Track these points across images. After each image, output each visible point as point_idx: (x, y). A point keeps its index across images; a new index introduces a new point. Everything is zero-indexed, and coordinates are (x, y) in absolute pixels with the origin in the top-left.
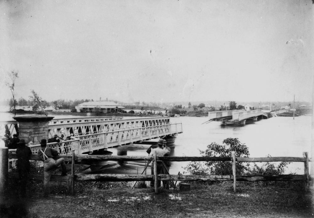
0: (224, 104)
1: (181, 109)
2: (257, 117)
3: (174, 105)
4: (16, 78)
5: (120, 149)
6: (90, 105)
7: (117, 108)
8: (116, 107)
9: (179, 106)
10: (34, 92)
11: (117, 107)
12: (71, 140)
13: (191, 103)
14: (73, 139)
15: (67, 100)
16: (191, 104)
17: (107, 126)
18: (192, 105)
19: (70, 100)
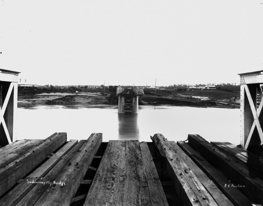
11: (33, 86)
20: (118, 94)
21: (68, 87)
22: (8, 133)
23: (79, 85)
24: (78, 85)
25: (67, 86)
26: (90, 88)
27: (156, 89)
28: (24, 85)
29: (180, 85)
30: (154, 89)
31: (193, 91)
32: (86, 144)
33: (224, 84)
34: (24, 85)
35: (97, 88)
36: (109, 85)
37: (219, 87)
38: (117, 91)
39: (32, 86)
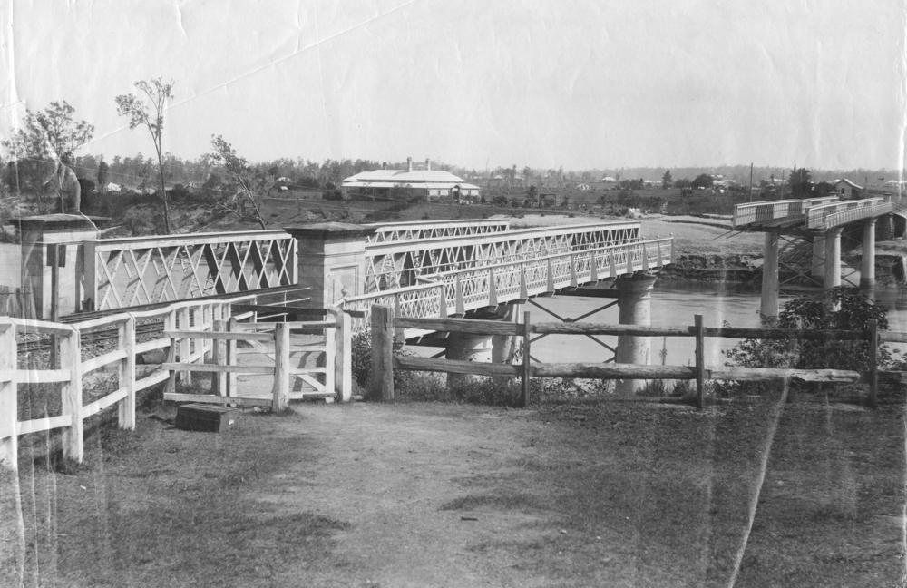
0: (772, 177)
1: (640, 191)
2: (876, 218)
3: (618, 177)
4: (661, 364)
5: (126, 190)
6: (678, 221)
7: (456, 189)
8: (454, 185)
9: (634, 181)
10: (445, 508)
11: (456, 187)
12: (417, 286)
13: (671, 173)
14: (422, 282)
15: (300, 162)
16: (672, 178)
17: (489, 247)
18: (674, 179)
19: (309, 163)
28: (424, 182)
29: (511, 168)
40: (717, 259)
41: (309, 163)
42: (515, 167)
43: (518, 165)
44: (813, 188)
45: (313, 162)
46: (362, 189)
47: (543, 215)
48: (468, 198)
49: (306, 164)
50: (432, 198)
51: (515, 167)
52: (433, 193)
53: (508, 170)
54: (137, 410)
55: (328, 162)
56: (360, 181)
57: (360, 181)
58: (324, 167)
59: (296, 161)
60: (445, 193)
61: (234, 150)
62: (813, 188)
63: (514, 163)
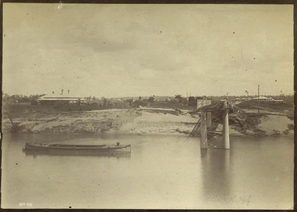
11: (79, 100)
20: (200, 108)
21: (120, 100)
22: (169, 209)
23: (140, 97)
24: (139, 96)
25: (119, 99)
26: (158, 101)
27: (268, 100)
28: (68, 98)
29: (89, 97)
30: (264, 100)
31: (17, 100)
32: (25, 125)
33: (94, 98)
34: (68, 98)
35: (170, 102)
36: (189, 96)
37: (111, 99)
38: (198, 105)
39: (78, 99)
40: (115, 98)
41: (25, 96)
42: (90, 96)
43: (91, 96)
44: (195, 99)
45: (26, 95)
46: (45, 101)
47: (165, 114)
48: (83, 103)
49: (23, 97)
50: (71, 103)
51: (90, 96)
52: (71, 102)
53: (88, 97)
54: (229, 129)
55: (31, 95)
56: (45, 98)
57: (45, 98)
58: (30, 97)
59: (20, 95)
60: (75, 102)
61: (102, 97)
62: (195, 99)
63: (90, 95)
